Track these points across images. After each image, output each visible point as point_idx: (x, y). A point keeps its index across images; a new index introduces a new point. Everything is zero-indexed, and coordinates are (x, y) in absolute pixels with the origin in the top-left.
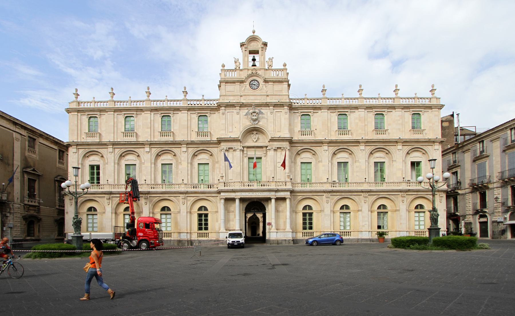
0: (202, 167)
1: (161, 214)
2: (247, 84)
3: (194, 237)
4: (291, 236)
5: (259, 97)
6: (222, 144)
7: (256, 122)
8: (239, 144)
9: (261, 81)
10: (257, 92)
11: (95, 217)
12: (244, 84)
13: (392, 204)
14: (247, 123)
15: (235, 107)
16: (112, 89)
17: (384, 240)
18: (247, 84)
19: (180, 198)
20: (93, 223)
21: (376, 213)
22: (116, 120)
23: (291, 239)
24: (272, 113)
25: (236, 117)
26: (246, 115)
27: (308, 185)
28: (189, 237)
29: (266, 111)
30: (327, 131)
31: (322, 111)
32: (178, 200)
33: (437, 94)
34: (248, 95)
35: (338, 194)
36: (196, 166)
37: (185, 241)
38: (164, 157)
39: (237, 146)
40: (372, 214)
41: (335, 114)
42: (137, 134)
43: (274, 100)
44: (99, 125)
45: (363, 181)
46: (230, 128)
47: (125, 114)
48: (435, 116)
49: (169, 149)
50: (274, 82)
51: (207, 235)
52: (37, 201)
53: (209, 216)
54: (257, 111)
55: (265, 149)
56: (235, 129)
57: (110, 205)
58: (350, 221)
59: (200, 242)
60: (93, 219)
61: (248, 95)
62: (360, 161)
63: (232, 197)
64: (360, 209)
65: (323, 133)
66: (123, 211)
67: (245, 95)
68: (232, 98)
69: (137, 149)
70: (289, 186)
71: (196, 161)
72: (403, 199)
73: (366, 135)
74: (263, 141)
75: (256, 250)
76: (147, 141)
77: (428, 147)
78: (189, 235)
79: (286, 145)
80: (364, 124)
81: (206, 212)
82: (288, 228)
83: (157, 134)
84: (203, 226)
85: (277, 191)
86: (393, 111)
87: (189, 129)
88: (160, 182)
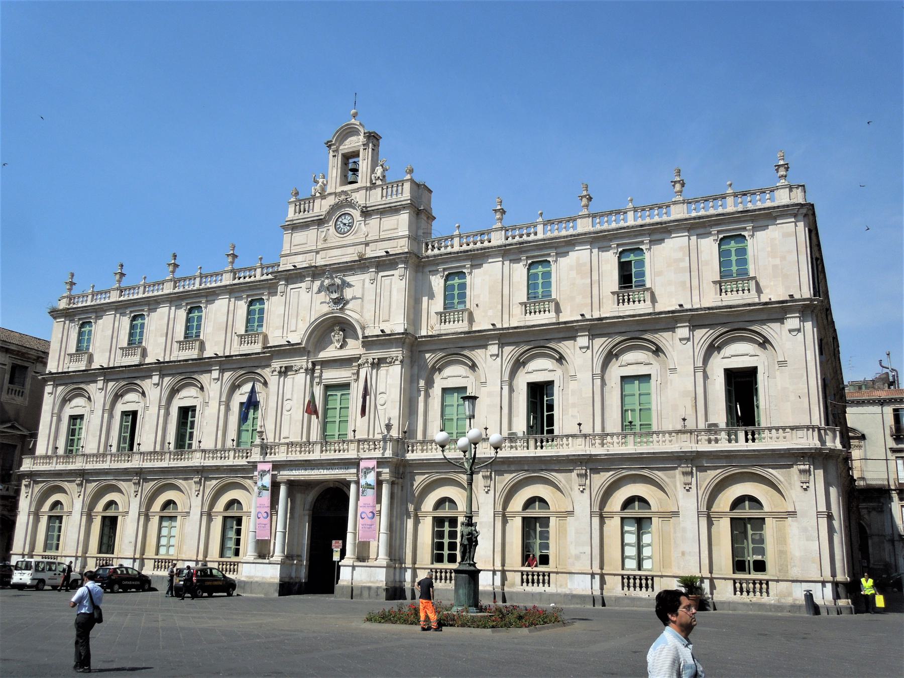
5: (350, 250)
10: (350, 239)
16: (175, 256)
21: (617, 521)
24: (373, 281)
25: (305, 297)
26: (319, 291)
28: (136, 567)
32: (569, 481)
39: (301, 362)
42: (471, 315)
43: (375, 251)
45: (575, 430)
46: (293, 321)
51: (545, 578)
57: (81, 497)
65: (490, 313)
66: (618, 508)
68: (300, 258)
71: (616, 371)
74: (354, 348)
81: (755, 514)
83: (518, 310)
84: (446, 552)
88: (61, 451)
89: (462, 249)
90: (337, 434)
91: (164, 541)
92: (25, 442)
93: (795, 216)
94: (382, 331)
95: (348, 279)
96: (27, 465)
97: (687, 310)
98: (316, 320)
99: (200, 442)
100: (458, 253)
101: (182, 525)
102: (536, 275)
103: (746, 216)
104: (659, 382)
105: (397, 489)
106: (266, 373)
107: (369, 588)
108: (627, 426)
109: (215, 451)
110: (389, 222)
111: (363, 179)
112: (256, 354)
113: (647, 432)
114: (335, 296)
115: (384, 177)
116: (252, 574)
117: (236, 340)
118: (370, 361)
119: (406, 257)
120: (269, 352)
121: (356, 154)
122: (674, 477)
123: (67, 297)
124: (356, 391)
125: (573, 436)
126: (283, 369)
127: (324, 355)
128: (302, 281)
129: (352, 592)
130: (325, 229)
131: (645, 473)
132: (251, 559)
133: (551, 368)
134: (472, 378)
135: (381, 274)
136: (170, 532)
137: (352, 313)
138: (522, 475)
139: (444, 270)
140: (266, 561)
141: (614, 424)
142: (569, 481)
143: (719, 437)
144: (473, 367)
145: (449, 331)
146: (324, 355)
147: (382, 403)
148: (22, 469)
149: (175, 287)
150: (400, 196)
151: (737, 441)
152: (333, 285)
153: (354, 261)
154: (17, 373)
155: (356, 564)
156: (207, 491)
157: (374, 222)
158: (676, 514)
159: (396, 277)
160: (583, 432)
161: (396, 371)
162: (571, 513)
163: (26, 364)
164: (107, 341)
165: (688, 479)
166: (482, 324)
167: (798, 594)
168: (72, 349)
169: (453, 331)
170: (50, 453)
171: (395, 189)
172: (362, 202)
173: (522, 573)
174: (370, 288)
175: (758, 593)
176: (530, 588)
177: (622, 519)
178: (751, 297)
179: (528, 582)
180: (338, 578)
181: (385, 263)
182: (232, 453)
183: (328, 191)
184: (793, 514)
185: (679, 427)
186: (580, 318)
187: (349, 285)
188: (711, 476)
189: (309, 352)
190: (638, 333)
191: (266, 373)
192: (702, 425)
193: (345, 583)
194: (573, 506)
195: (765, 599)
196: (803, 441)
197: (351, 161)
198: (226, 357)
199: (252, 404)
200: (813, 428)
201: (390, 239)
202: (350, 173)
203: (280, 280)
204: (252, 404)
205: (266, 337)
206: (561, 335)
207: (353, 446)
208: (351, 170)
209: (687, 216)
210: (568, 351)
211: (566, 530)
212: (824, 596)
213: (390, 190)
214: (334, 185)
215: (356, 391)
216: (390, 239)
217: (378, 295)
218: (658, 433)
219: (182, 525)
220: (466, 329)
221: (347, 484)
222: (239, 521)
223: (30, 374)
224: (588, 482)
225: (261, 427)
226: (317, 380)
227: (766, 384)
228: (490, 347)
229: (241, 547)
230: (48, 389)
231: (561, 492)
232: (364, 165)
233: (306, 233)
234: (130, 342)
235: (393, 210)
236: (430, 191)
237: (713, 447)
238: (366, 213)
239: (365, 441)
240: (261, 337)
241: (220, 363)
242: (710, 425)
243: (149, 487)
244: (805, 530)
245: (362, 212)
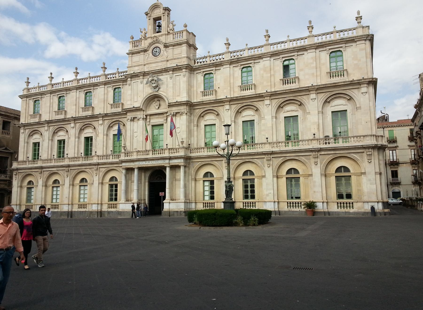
0: (208, 129)
1: (204, 181)
2: (150, 52)
3: (105, 208)
4: (183, 207)
5: (160, 64)
6: (128, 114)
7: (157, 89)
8: (142, 112)
9: (161, 46)
10: (159, 59)
11: (86, 188)
12: (148, 52)
13: (304, 167)
14: (149, 91)
15: (139, 76)
17: (314, 213)
18: (150, 52)
19: (265, 160)
20: (84, 194)
22: (51, 101)
23: (183, 210)
24: (171, 78)
25: (141, 86)
26: (147, 83)
27: (206, 150)
29: (166, 76)
30: (229, 88)
31: (224, 67)
32: (263, 163)
33: (364, 23)
34: (150, 63)
35: (238, 158)
36: (203, 127)
37: (96, 212)
38: (288, 108)
39: (140, 115)
40: (279, 180)
41: (238, 68)
42: (66, 112)
43: (172, 64)
44: (122, 95)
45: (265, 141)
46: (136, 97)
47: (58, 95)
48: (361, 50)
49: (90, 123)
50: (174, 45)
52: (8, 176)
53: (256, 180)
54: (155, 78)
55: (165, 115)
57: (42, 178)
58: (204, 191)
59: (109, 212)
60: (57, 191)
61: (150, 63)
62: (266, 117)
63: (131, 167)
64: (363, 171)
66: (51, 184)
67: (148, 64)
68: (136, 68)
69: (40, 128)
70: (182, 153)
72: (316, 160)
73: (273, 86)
75: (152, 221)
76: (72, 117)
77: (353, 90)
78: (99, 206)
79: (184, 109)
80: (269, 75)
81: (251, 177)
82: (182, 197)
83: (237, 89)
84: (249, 194)
85: (170, 158)
86: (305, 53)
87: (106, 102)
88: (30, 159)
89: (211, 62)
91: (82, 196)
92: (13, 154)
96: (15, 165)
98: (146, 96)
100: (209, 64)
103: (90, 85)
104: (302, 119)
105: (187, 169)
106: (124, 120)
107: (177, 211)
108: (288, 138)
109: (103, 156)
111: (164, 30)
112: (119, 112)
113: (346, 138)
114: (154, 85)
115: (174, 29)
116: (124, 208)
117: (109, 106)
120: (125, 111)
121: (159, 18)
123: (27, 89)
124: (167, 127)
125: (265, 143)
126: (175, 114)
129: (170, 213)
132: (123, 202)
133: (253, 114)
135: (175, 75)
136: (84, 192)
137: (162, 92)
141: (282, 137)
142: (263, 163)
143: (330, 141)
145: (207, 100)
148: (12, 167)
149: (78, 83)
151: (244, 149)
154: (6, 125)
155: (170, 202)
156: (44, 177)
158: (311, 175)
159: (182, 76)
160: (269, 142)
161: (184, 118)
162: (264, 176)
163: (9, 121)
164: (48, 109)
166: (221, 96)
167: (367, 208)
168: (31, 112)
169: (208, 99)
170: (25, 160)
172: (164, 41)
174: (170, 81)
175: (348, 208)
180: (163, 208)
181: (177, 69)
182: (111, 157)
184: (364, 173)
185: (312, 138)
188: (277, 162)
191: (124, 120)
192: (322, 137)
193: (166, 210)
195: (352, 210)
196: (368, 142)
197: (157, 22)
198: (105, 114)
199: (119, 133)
200: (374, 135)
202: (157, 28)
204: (119, 133)
205: (123, 104)
207: (167, 151)
208: (158, 26)
210: (261, 107)
211: (262, 184)
212: (379, 207)
214: (150, 33)
215: (167, 127)
217: (174, 85)
219: (90, 189)
220: (215, 99)
221: (165, 168)
222: (116, 186)
223: (12, 125)
224: (271, 163)
225: (124, 144)
227: (351, 117)
229: (118, 197)
230: (22, 131)
232: (163, 23)
234: (59, 109)
235: (180, 44)
236: (195, 36)
237: (327, 146)
239: (172, 149)
240: (121, 105)
242: (326, 137)
244: (370, 180)
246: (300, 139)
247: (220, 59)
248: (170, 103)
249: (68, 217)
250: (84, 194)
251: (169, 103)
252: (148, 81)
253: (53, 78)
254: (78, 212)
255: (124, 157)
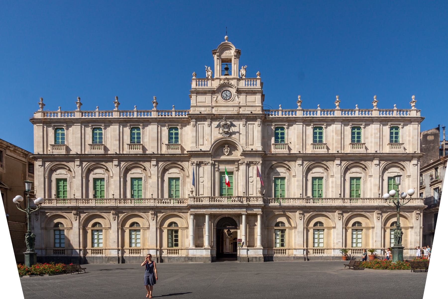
0: (136, 182)
5: (231, 109)
10: (230, 103)
20: (357, 239)
39: (209, 160)
51: (176, 251)
54: (228, 123)
56: (206, 142)
57: (78, 220)
59: (169, 258)
68: (202, 109)
81: (176, 228)
90: (227, 194)
93: (418, 122)
94: (201, 150)
95: (234, 123)
97: (379, 154)
99: (74, 195)
101: (143, 234)
102: (134, 133)
107: (256, 257)
110: (250, 98)
113: (102, 198)
118: (246, 162)
119: (262, 116)
120: (190, 154)
122: (373, 215)
126: (198, 163)
127: (223, 158)
128: (204, 121)
130: (216, 96)
131: (363, 213)
134: (69, 175)
138: (315, 213)
139: (391, 124)
140: (203, 248)
144: (183, 169)
146: (223, 158)
147: (252, 181)
150: (255, 86)
152: (226, 124)
153: (235, 115)
157: (242, 97)
165: (379, 216)
169: (281, 153)
171: (252, 82)
173: (168, 250)
176: (316, 255)
177: (130, 230)
178: (363, 151)
179: (170, 253)
181: (250, 118)
183: (215, 78)
186: (337, 152)
187: (234, 126)
189: (212, 156)
190: (173, 161)
194: (110, 226)
201: (252, 106)
203: (192, 119)
206: (328, 159)
209: (379, 116)
213: (249, 82)
216: (252, 106)
217: (247, 133)
218: (106, 200)
226: (216, 169)
228: (336, 161)
231: (330, 219)
232: (234, 67)
233: (205, 97)
235: (253, 93)
238: (239, 92)
241: (157, 158)
243: (385, 215)
245: (237, 90)
246: (324, 197)
247: (162, 116)
248: (245, 151)
249: (119, 263)
250: (357, 239)
251: (243, 151)
252: (219, 124)
253: (44, 105)
254: (129, 257)
255: (193, 202)
